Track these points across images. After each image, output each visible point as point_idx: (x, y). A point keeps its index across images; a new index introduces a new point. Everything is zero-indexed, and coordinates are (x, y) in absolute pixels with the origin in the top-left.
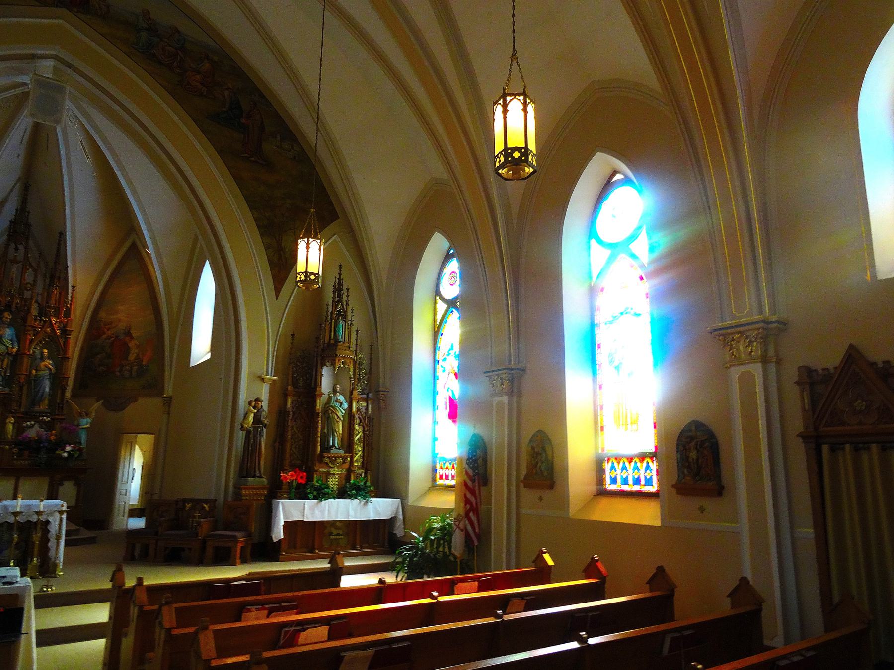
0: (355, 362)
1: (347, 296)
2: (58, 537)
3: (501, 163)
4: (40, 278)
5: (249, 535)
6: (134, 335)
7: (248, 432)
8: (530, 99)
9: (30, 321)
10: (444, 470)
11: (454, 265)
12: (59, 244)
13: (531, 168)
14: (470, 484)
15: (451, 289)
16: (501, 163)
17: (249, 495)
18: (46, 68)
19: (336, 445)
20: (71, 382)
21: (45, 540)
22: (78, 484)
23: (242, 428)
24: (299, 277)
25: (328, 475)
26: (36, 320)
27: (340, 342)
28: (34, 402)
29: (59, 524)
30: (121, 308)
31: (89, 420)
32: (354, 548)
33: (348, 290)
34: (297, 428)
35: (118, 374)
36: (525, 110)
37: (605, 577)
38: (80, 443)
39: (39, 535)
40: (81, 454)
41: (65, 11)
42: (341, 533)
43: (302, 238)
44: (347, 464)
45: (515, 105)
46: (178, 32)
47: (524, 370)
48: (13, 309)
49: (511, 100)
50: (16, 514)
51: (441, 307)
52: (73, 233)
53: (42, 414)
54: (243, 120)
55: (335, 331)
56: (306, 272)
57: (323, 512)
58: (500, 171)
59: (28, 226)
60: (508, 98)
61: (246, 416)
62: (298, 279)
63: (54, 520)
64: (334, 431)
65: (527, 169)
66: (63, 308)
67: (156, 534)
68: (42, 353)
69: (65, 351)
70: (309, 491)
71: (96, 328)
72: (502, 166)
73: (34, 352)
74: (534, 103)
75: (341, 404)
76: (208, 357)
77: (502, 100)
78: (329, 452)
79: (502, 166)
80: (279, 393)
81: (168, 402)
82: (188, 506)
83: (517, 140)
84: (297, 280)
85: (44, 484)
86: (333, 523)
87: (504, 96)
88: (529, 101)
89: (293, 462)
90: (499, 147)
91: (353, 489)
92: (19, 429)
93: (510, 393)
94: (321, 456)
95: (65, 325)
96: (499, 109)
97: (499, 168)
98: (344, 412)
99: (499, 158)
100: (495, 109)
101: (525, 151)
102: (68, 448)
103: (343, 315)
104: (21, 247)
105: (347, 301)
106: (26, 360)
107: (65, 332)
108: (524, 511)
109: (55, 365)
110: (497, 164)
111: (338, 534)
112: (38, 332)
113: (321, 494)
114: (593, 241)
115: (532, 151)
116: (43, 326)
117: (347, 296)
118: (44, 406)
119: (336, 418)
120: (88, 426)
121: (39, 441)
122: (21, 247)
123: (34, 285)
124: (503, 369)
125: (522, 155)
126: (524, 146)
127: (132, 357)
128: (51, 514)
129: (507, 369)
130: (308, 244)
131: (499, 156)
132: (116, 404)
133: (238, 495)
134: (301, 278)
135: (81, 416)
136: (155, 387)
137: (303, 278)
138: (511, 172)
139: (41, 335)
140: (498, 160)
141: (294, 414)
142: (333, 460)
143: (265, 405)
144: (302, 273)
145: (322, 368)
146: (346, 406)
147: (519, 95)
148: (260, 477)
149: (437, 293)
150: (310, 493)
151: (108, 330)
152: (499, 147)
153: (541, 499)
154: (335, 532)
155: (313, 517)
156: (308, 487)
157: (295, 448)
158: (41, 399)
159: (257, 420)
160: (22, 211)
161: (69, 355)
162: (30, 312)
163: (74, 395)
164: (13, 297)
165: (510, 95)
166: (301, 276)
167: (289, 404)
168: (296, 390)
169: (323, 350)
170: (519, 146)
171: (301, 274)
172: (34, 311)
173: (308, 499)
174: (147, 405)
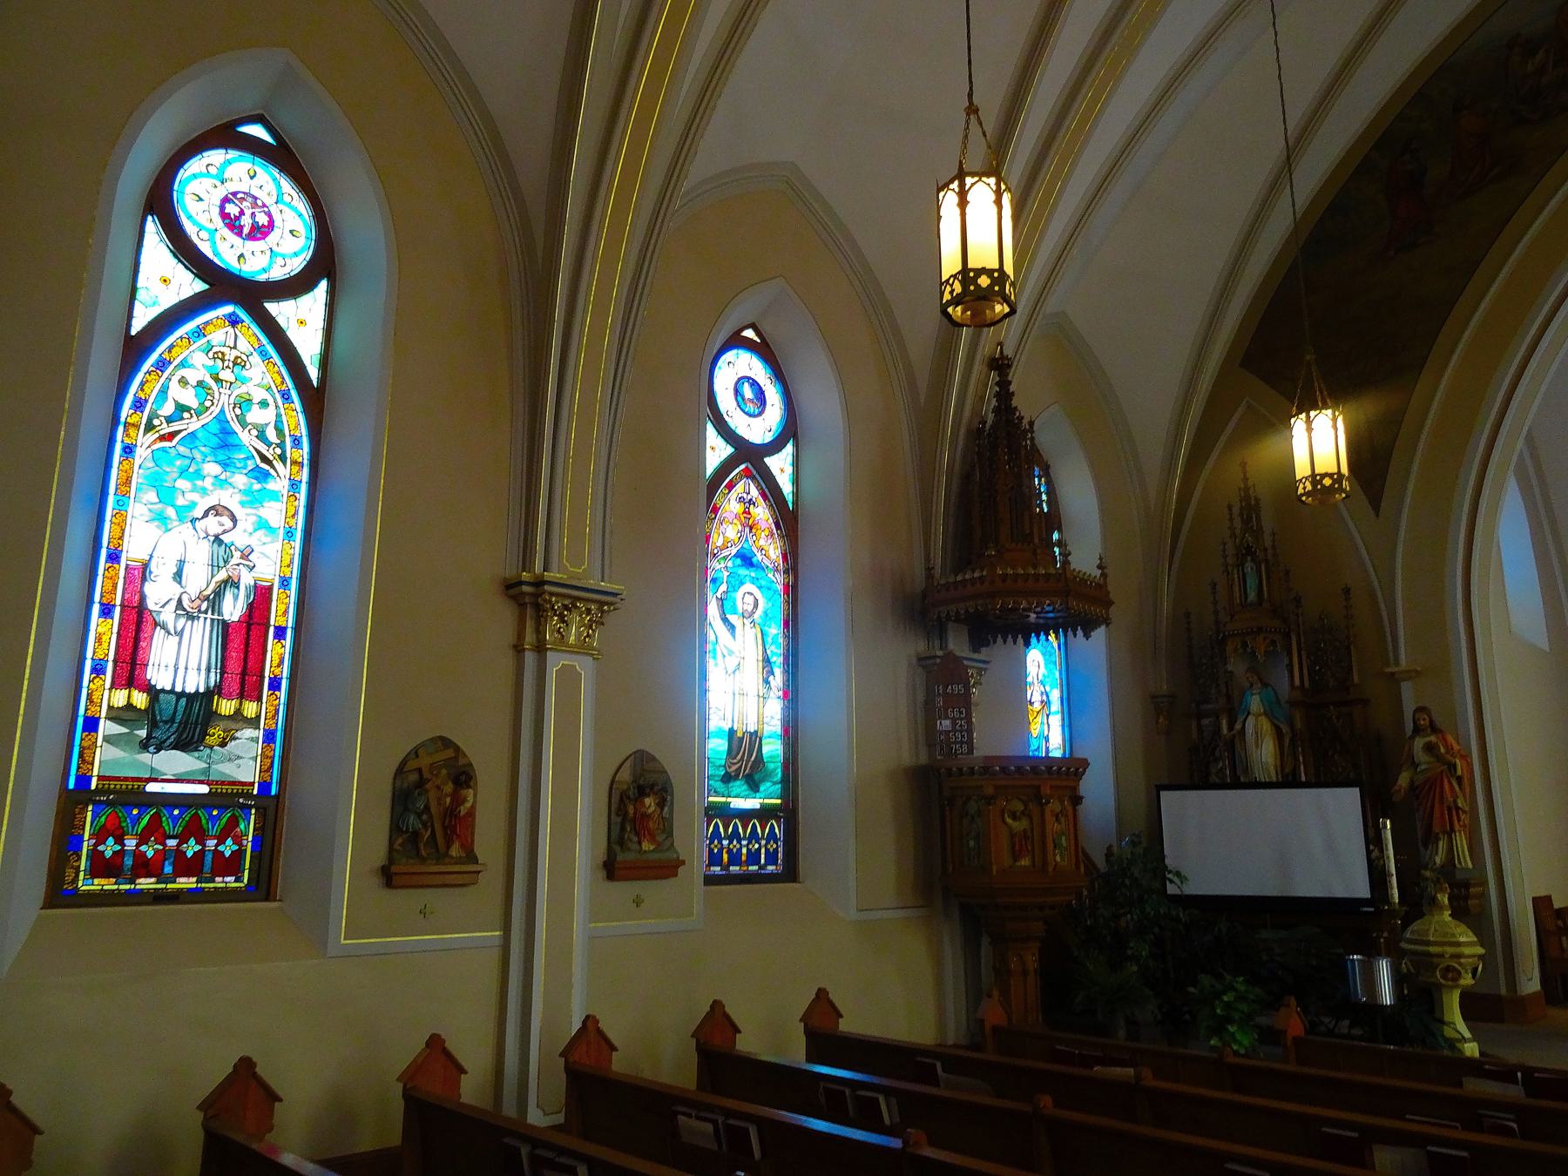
3: (955, 294)
8: (1005, 184)
16: (955, 294)
24: (1301, 486)
36: (1335, 428)
43: (1297, 414)
45: (982, 192)
49: (973, 185)
58: (950, 310)
60: (969, 181)
62: (1300, 491)
65: (998, 308)
72: (956, 301)
74: (1010, 191)
77: (956, 183)
79: (956, 301)
83: (984, 254)
84: (1299, 493)
87: (961, 176)
90: (950, 263)
96: (949, 200)
97: (949, 303)
99: (952, 285)
100: (941, 198)
101: (999, 276)
110: (947, 297)
125: (994, 282)
126: (997, 267)
130: (1309, 422)
131: (951, 281)
134: (1304, 488)
137: (1309, 487)
138: (969, 313)
140: (948, 289)
144: (1306, 478)
152: (950, 263)
165: (973, 175)
170: (1330, 471)
171: (1304, 480)
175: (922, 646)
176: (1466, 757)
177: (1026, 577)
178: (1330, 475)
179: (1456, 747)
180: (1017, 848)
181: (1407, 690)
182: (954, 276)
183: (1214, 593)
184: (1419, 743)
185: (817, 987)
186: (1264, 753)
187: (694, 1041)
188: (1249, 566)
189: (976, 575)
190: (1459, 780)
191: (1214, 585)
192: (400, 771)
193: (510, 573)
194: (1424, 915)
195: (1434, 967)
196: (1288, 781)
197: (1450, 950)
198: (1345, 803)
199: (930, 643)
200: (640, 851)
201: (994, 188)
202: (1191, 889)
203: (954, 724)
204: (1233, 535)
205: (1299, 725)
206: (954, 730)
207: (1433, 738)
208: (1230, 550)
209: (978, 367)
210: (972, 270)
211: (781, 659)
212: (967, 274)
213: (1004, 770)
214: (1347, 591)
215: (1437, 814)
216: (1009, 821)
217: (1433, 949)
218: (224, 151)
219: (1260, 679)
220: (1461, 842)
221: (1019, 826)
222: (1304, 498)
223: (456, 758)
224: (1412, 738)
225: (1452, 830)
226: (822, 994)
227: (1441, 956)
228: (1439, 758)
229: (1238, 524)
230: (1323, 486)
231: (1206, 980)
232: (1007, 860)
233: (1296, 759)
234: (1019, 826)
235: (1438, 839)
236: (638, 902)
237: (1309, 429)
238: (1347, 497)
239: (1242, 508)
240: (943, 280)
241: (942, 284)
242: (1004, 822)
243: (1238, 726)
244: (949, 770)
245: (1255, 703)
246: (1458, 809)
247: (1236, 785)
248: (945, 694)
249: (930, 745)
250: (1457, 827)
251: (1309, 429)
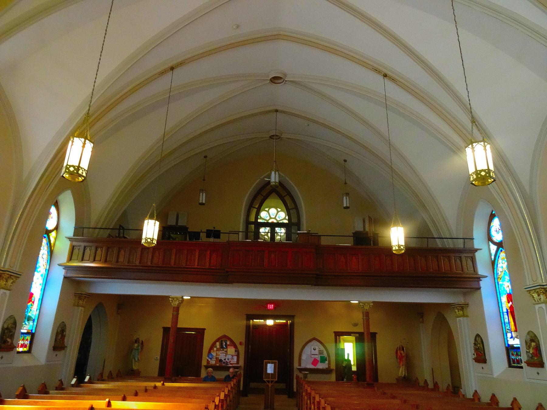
3: (474, 178)
8: (487, 143)
13: (492, 179)
36: (485, 150)
51: (493, 248)
62: (472, 179)
83: (482, 166)
84: (471, 180)
88: (487, 144)
90: (472, 170)
99: (473, 176)
101: (489, 171)
115: (492, 170)
126: (487, 168)
130: (473, 148)
137: (475, 177)
147: (481, 142)
166: (473, 176)
170: (484, 169)
178: (484, 171)
182: (473, 173)
194: (527, 335)
199: (178, 256)
201: (483, 145)
210: (478, 171)
212: (477, 172)
218: (499, 224)
222: (474, 182)
236: (56, 355)
237: (473, 151)
238: (494, 180)
240: (470, 174)
241: (470, 175)
251: (473, 151)
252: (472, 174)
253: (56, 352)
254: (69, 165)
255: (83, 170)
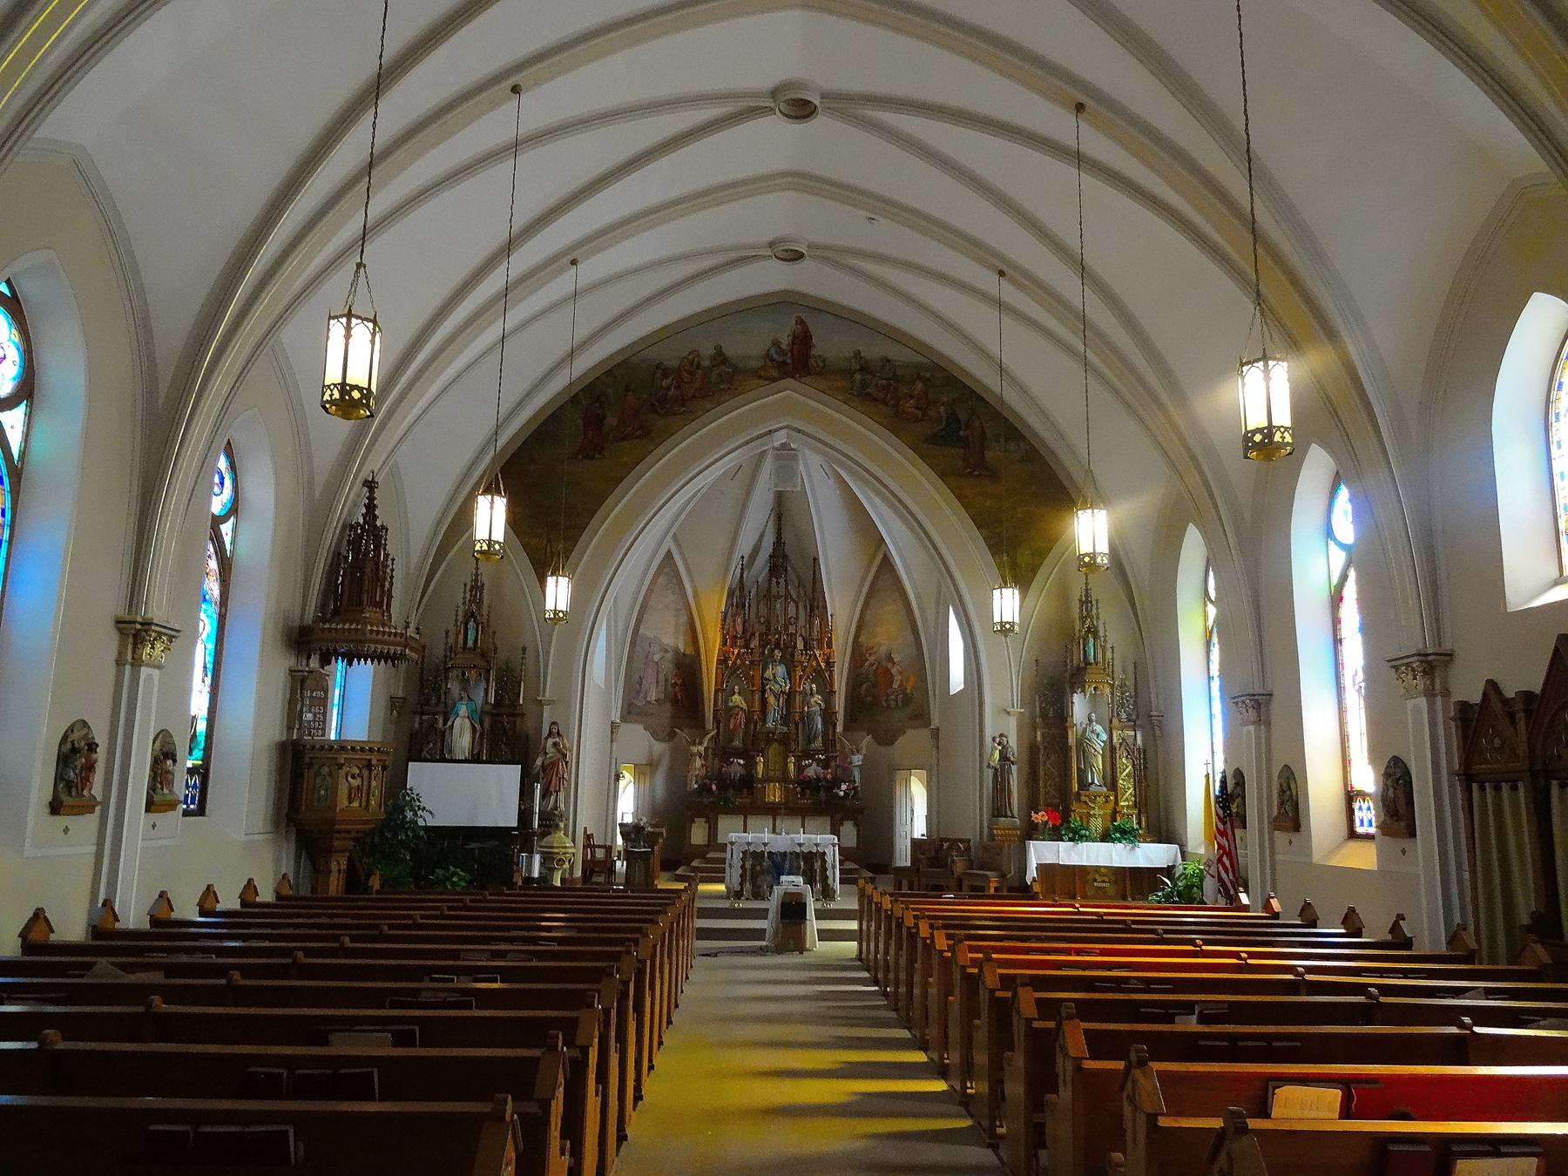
0: (1112, 686)
1: (1097, 608)
2: (834, 867)
4: (801, 611)
5: (1003, 876)
6: (895, 660)
7: (996, 769)
9: (798, 657)
10: (1365, 811)
11: (1344, 493)
12: (814, 572)
14: (1221, 826)
15: (1345, 529)
17: (1002, 835)
18: (780, 438)
19: (1096, 782)
20: (840, 717)
21: (824, 869)
22: (856, 824)
23: (989, 766)
25: (1089, 815)
26: (802, 654)
27: (1091, 664)
28: (810, 740)
29: (833, 857)
30: (879, 630)
31: (861, 757)
32: (1124, 898)
33: (1097, 600)
34: (1050, 764)
35: (884, 704)
37: (1342, 924)
38: (855, 782)
39: (819, 863)
40: (856, 792)
41: (789, 381)
42: (1107, 879)
44: (1112, 804)
46: (889, 361)
47: (1271, 695)
48: (782, 646)
50: (800, 845)
52: (826, 556)
53: (817, 751)
54: (962, 433)
55: (1085, 652)
56: (1001, 622)
57: (1080, 855)
59: (785, 557)
61: (992, 754)
63: (829, 851)
64: (1091, 766)
66: (825, 639)
67: (918, 870)
68: (811, 689)
69: (832, 685)
70: (1063, 832)
71: (858, 655)
73: (804, 688)
75: (1098, 735)
76: (962, 687)
78: (1088, 790)
80: (1028, 727)
81: (936, 734)
82: (946, 845)
84: (325, 399)
85: (826, 822)
86: (1097, 869)
89: (1049, 801)
90: (333, 376)
91: (1117, 832)
92: (800, 769)
93: (1258, 722)
94: (1078, 795)
95: (829, 658)
98: (1102, 744)
102: (844, 787)
103: (1093, 631)
104: (782, 581)
105: (1098, 614)
106: (798, 699)
107: (829, 664)
108: (1278, 857)
109: (825, 701)
111: (1103, 882)
112: (806, 667)
113: (1077, 836)
114: (1332, 543)
116: (809, 660)
117: (1097, 608)
118: (818, 744)
119: (1093, 751)
120: (860, 763)
121: (818, 779)
122: (782, 581)
123: (797, 619)
124: (1413, 656)
127: (895, 686)
128: (826, 847)
129: (1419, 655)
132: (886, 738)
133: (992, 837)
134: (331, 395)
135: (853, 753)
136: (920, 717)
137: (337, 395)
139: (808, 670)
141: (1045, 748)
142: (1094, 798)
143: (1013, 742)
144: (335, 385)
145: (1072, 696)
146: (1104, 737)
148: (1013, 817)
149: (1329, 533)
150: (1064, 835)
151: (870, 655)
153: (1290, 842)
154: (1099, 879)
155: (1069, 860)
156: (1062, 828)
157: (1050, 786)
158: (815, 737)
159: (1004, 757)
160: (779, 543)
161: (836, 687)
162: (796, 647)
163: (846, 728)
164: (780, 634)
167: (1039, 738)
168: (1046, 721)
169: (1072, 676)
172: (800, 645)
173: (1062, 840)
174: (912, 740)
175: (291, 662)
176: (571, 751)
177: (378, 632)
179: (568, 746)
180: (353, 796)
181: (547, 709)
183: (447, 637)
184: (550, 741)
185: (165, 890)
186: (462, 737)
187: (20, 940)
188: (471, 624)
189: (346, 626)
190: (567, 763)
191: (447, 632)
192: (65, 738)
193: (121, 612)
195: (554, 859)
196: (475, 759)
197: (563, 850)
198: (511, 774)
200: (163, 794)
202: (431, 822)
203: (315, 715)
204: (464, 603)
205: (486, 725)
206: (314, 721)
207: (557, 739)
208: (461, 613)
209: (359, 483)
211: (212, 666)
213: (353, 749)
214: (524, 649)
215: (553, 783)
216: (350, 779)
217: (555, 851)
219: (468, 696)
220: (562, 795)
221: (355, 783)
222: (327, 406)
223: (87, 734)
224: (546, 738)
225: (559, 790)
226: (250, 881)
227: (558, 853)
228: (559, 751)
229: (468, 595)
230: (352, 397)
231: (439, 872)
232: (346, 803)
233: (481, 745)
234: (355, 783)
235: (551, 795)
236: (66, 830)
237: (348, 336)
239: (472, 586)
241: (324, 386)
242: (347, 780)
243: (449, 723)
244: (313, 747)
245: (463, 709)
246: (564, 778)
247: (443, 760)
248: (312, 696)
249: (290, 728)
250: (562, 789)
252: (332, 387)
253: (155, 817)
254: (349, 385)
255: (1282, 430)
